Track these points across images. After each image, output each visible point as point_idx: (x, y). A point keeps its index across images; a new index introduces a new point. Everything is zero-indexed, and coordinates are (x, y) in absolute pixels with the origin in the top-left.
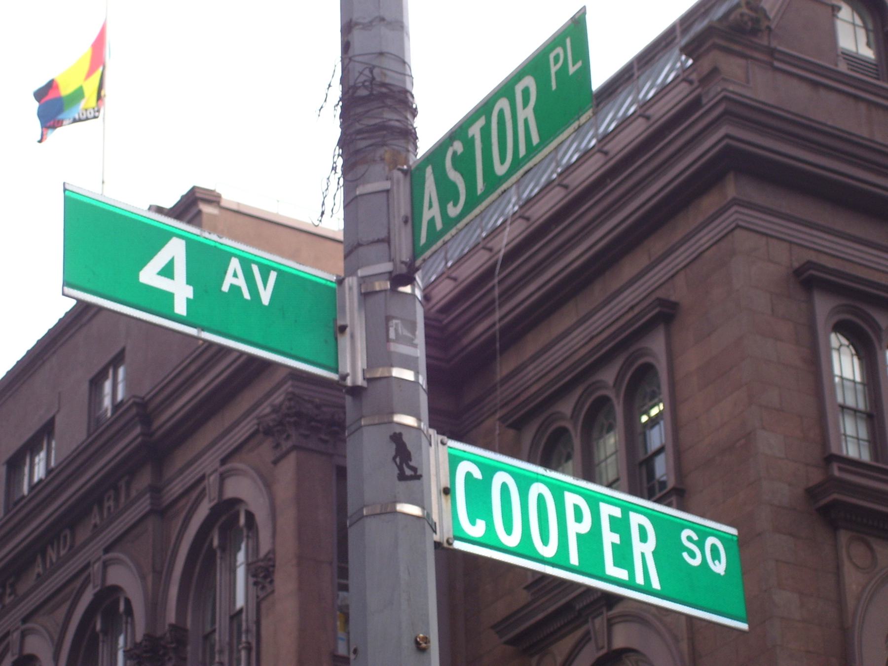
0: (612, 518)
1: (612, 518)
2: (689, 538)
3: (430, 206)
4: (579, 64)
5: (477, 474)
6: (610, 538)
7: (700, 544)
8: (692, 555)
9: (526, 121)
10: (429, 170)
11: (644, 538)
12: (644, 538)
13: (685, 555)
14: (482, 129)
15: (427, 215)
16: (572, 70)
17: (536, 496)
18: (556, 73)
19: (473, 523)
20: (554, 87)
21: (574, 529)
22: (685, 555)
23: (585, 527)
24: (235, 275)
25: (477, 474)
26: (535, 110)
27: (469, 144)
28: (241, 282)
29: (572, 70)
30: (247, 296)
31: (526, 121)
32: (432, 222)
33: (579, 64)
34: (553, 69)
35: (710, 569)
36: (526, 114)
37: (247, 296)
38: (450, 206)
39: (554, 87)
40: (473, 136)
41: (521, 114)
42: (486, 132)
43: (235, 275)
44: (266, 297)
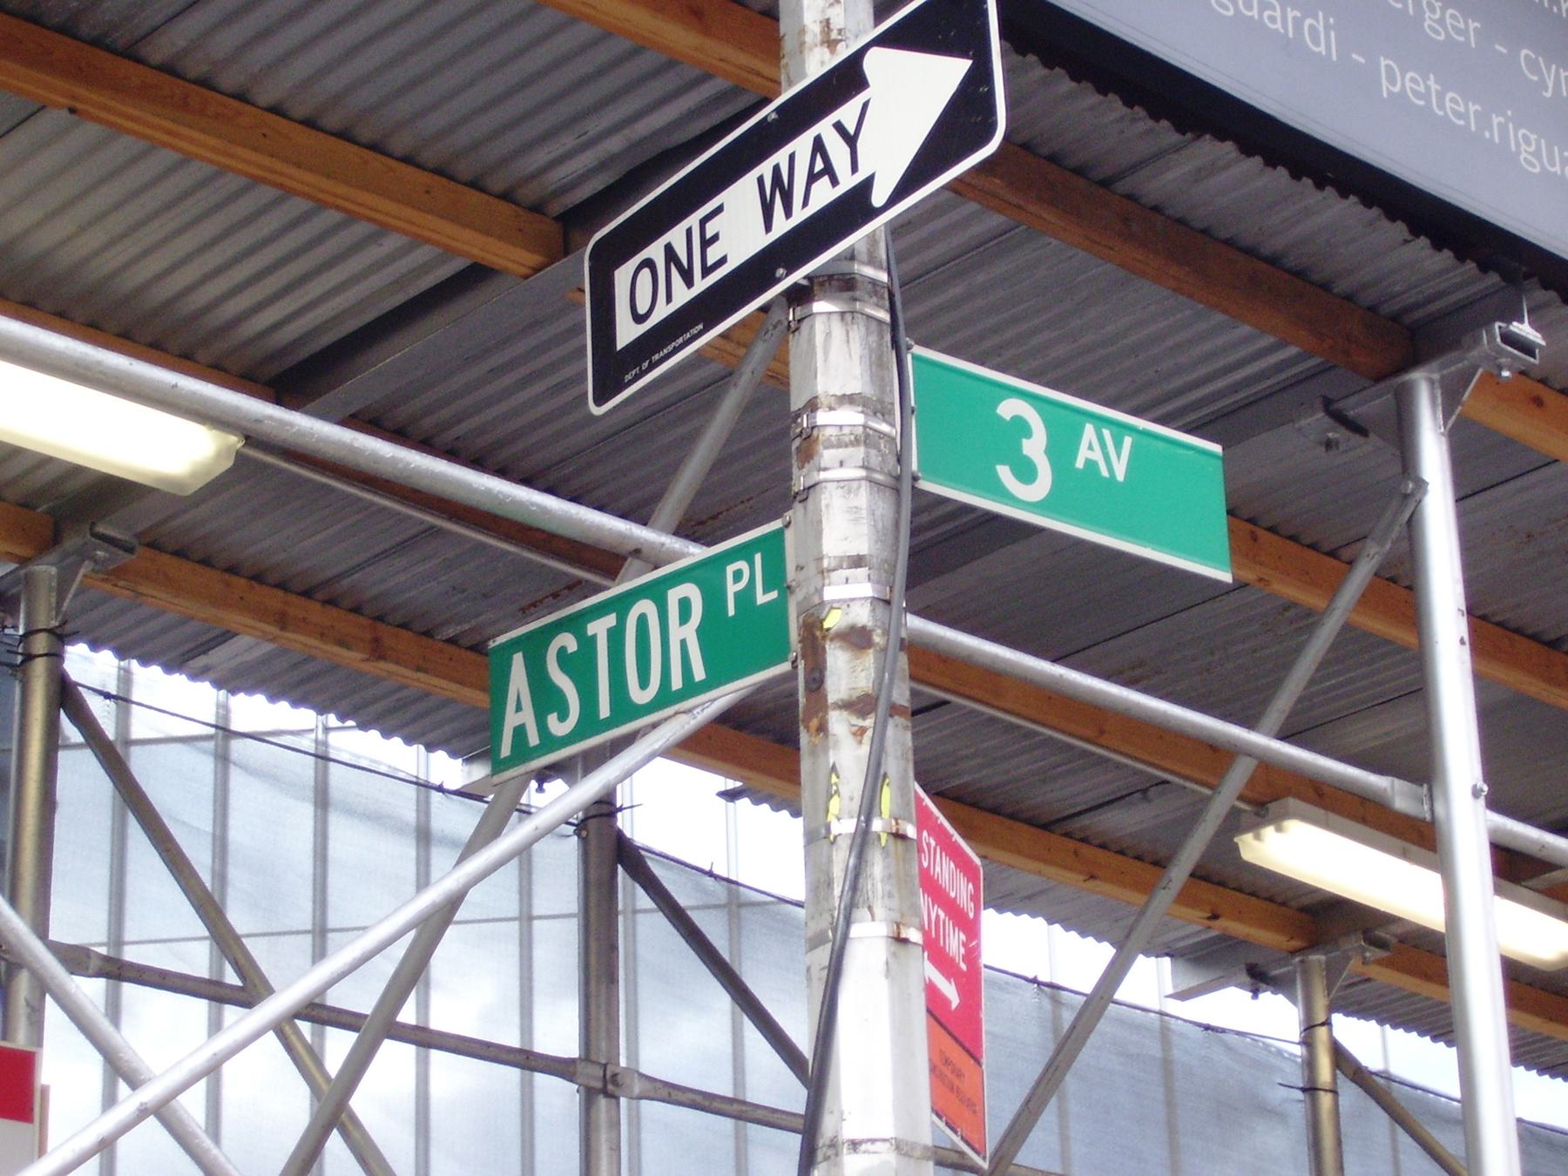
3: (519, 708)
4: (774, 595)
8: (1533, 166)
9: (683, 643)
10: (518, 660)
14: (610, 632)
15: (511, 720)
16: (762, 598)
17: (922, 986)
18: (736, 594)
20: (731, 612)
24: (1090, 448)
26: (701, 632)
27: (588, 644)
28: (1097, 455)
29: (762, 598)
31: (683, 643)
32: (520, 731)
33: (774, 595)
34: (732, 589)
36: (686, 633)
37: (1105, 473)
38: (552, 719)
39: (731, 612)
40: (594, 637)
41: (677, 633)
42: (616, 636)
43: (1090, 448)
44: (1120, 477)
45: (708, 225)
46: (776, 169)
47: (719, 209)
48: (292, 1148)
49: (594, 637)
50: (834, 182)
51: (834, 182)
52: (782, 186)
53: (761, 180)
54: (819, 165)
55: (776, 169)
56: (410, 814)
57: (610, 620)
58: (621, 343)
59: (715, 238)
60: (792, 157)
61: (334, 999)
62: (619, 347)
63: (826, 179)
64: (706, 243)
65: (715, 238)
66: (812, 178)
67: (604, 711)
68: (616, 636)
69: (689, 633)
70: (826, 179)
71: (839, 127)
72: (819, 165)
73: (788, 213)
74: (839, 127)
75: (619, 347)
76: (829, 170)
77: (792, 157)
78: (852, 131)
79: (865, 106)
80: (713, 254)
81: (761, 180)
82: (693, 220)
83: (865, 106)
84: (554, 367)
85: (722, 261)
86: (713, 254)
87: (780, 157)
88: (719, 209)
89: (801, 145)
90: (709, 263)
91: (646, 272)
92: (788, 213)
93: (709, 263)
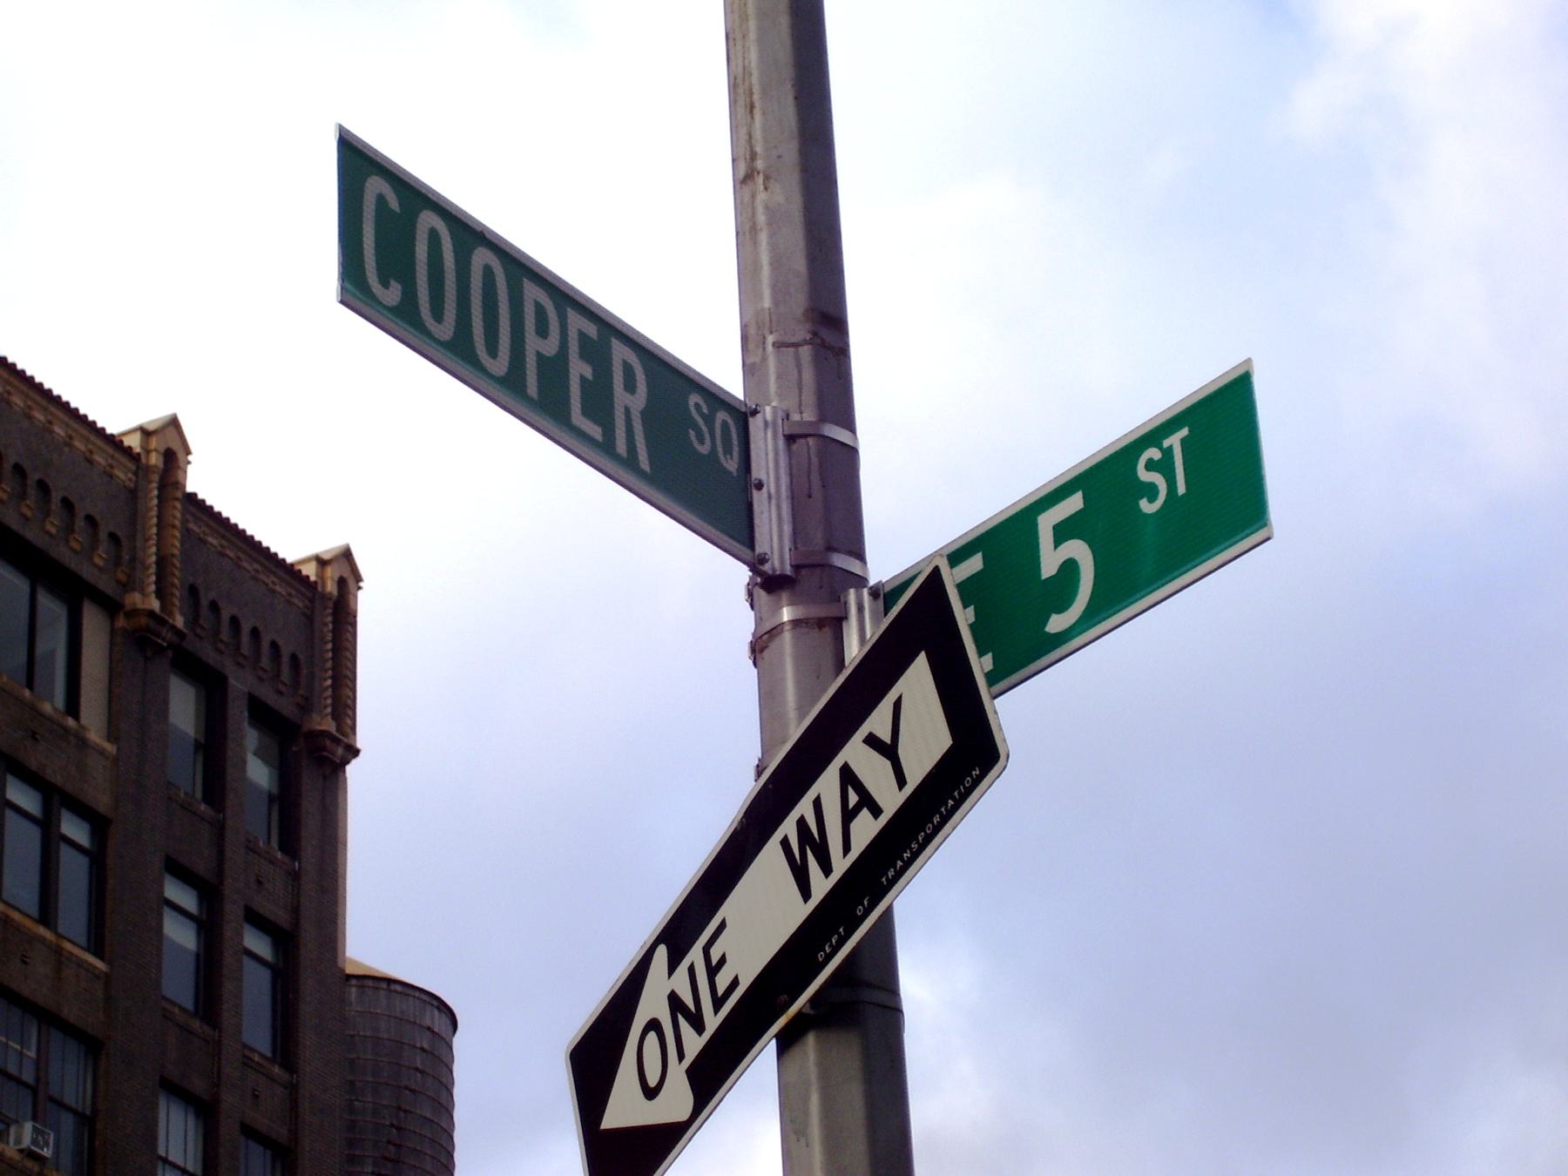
0: (582, 335)
1: (582, 335)
2: (697, 406)
5: (394, 204)
6: (579, 369)
7: (709, 420)
11: (630, 386)
12: (630, 386)
13: (692, 433)
19: (386, 285)
21: (533, 344)
22: (692, 433)
23: (550, 347)
25: (394, 204)
30: (1184, 432)
35: (1135, 473)
45: (712, 951)
46: (802, 823)
47: (722, 926)
48: (84, 651)
50: (876, 811)
51: (876, 811)
52: (814, 841)
53: (785, 843)
54: (853, 798)
55: (802, 823)
58: (921, 664)
59: (723, 960)
60: (817, 804)
61: (34, 910)
62: (923, 654)
63: (865, 812)
64: (712, 971)
65: (723, 960)
66: (848, 816)
70: (865, 812)
71: (872, 741)
72: (853, 798)
73: (827, 869)
74: (872, 741)
75: (923, 654)
76: (868, 802)
77: (817, 804)
79: (897, 705)
81: (785, 843)
83: (897, 705)
87: (804, 808)
88: (722, 926)
89: (827, 785)
90: (720, 992)
91: (652, 1036)
92: (827, 869)
93: (720, 992)
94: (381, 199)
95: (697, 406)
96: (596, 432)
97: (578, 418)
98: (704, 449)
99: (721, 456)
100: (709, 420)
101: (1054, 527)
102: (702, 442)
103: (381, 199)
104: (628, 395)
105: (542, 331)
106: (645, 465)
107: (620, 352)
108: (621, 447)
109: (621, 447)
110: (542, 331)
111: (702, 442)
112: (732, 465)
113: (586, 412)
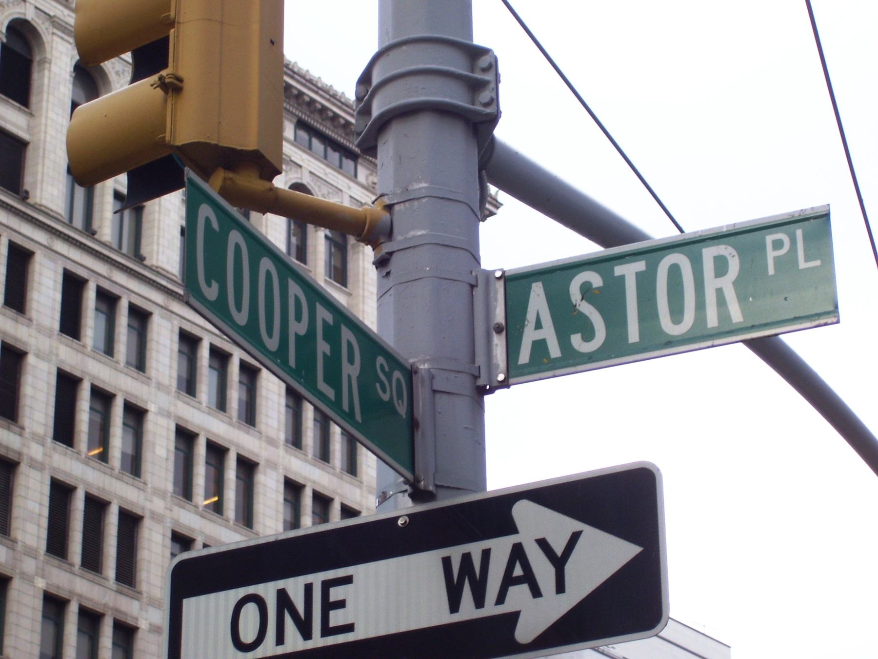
2: (382, 366)
5: (215, 225)
6: (323, 347)
7: (389, 376)
11: (351, 361)
12: (351, 361)
13: (378, 385)
19: (209, 285)
22: (378, 385)
25: (215, 225)
26: (736, 283)
31: (719, 292)
40: (622, 278)
41: (711, 283)
42: (646, 283)
49: (622, 278)
56: (166, 426)
57: (640, 266)
64: (328, 606)
65: (341, 604)
66: (509, 580)
67: (633, 335)
68: (646, 283)
69: (727, 283)
70: (525, 588)
72: (518, 571)
78: (559, 550)
80: (337, 618)
82: (317, 579)
84: (217, 486)
85: (349, 628)
86: (337, 618)
88: (348, 580)
94: (208, 221)
95: (382, 366)
96: (330, 393)
97: (322, 386)
98: (386, 397)
99: (396, 404)
100: (389, 376)
101: (733, 283)
102: (384, 391)
103: (208, 221)
104: (349, 365)
105: (298, 318)
106: (292, 362)
107: (346, 334)
108: (346, 406)
109: (346, 406)
110: (298, 318)
111: (384, 391)
112: (402, 409)
113: (326, 380)
